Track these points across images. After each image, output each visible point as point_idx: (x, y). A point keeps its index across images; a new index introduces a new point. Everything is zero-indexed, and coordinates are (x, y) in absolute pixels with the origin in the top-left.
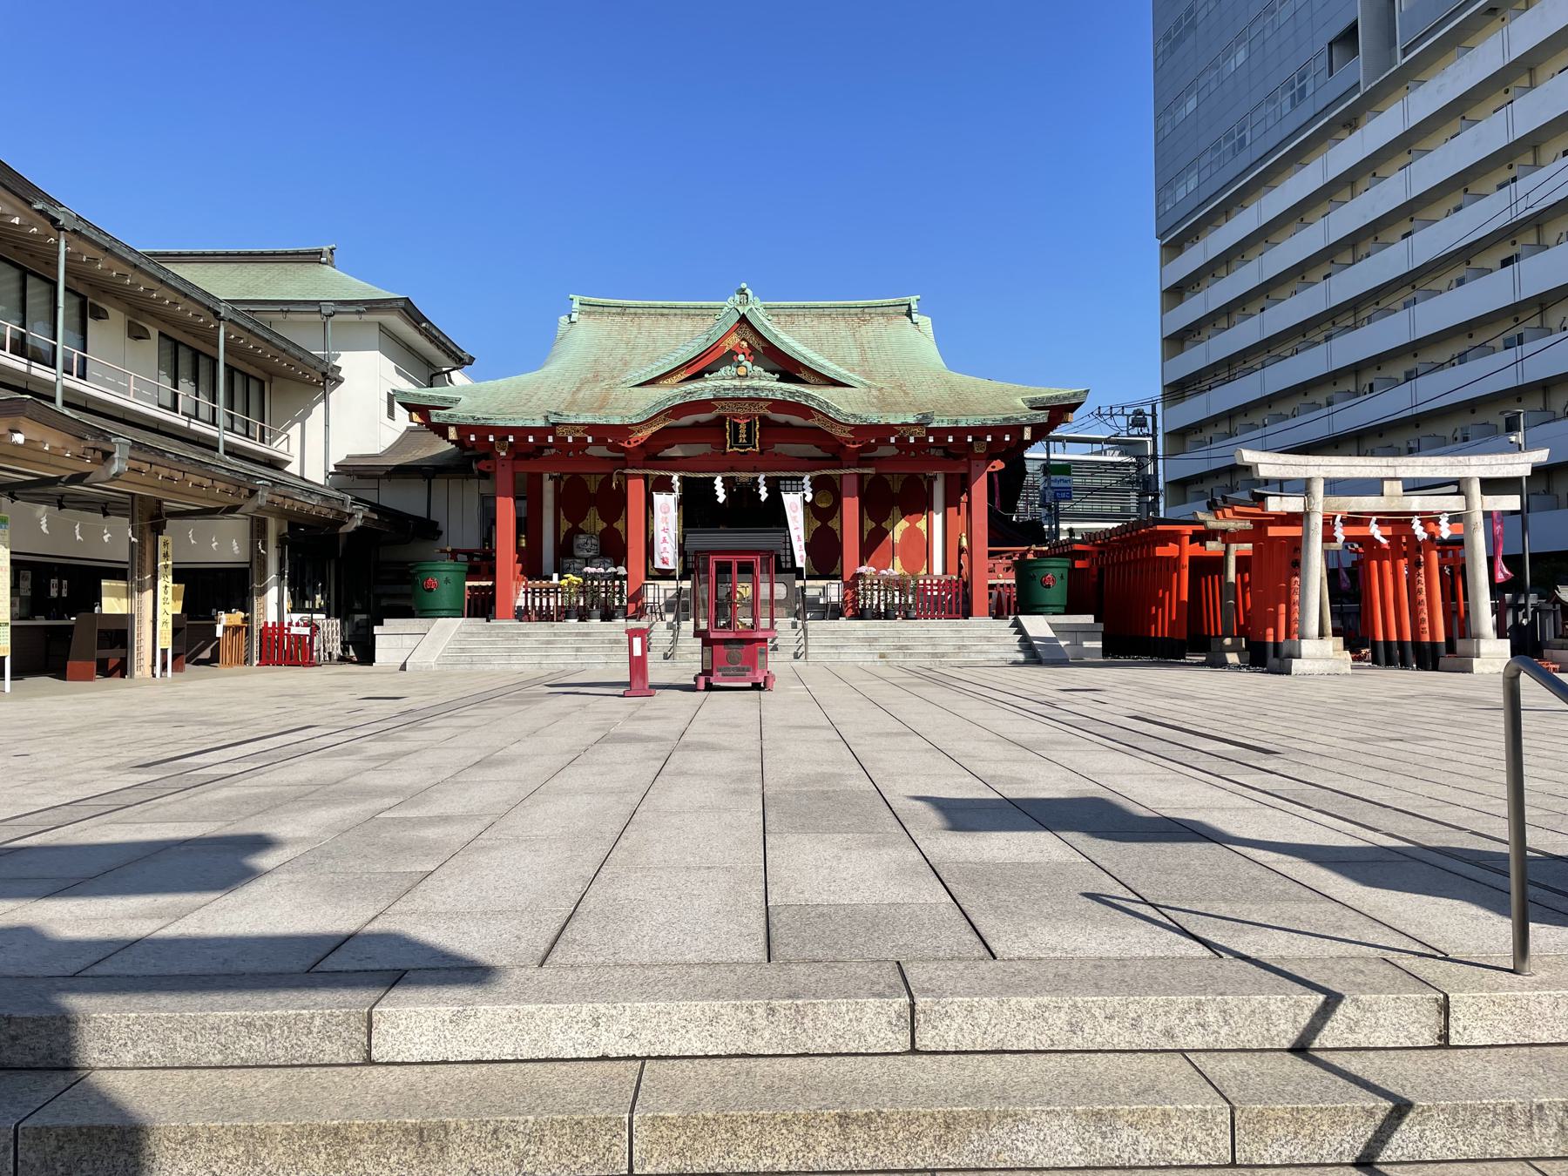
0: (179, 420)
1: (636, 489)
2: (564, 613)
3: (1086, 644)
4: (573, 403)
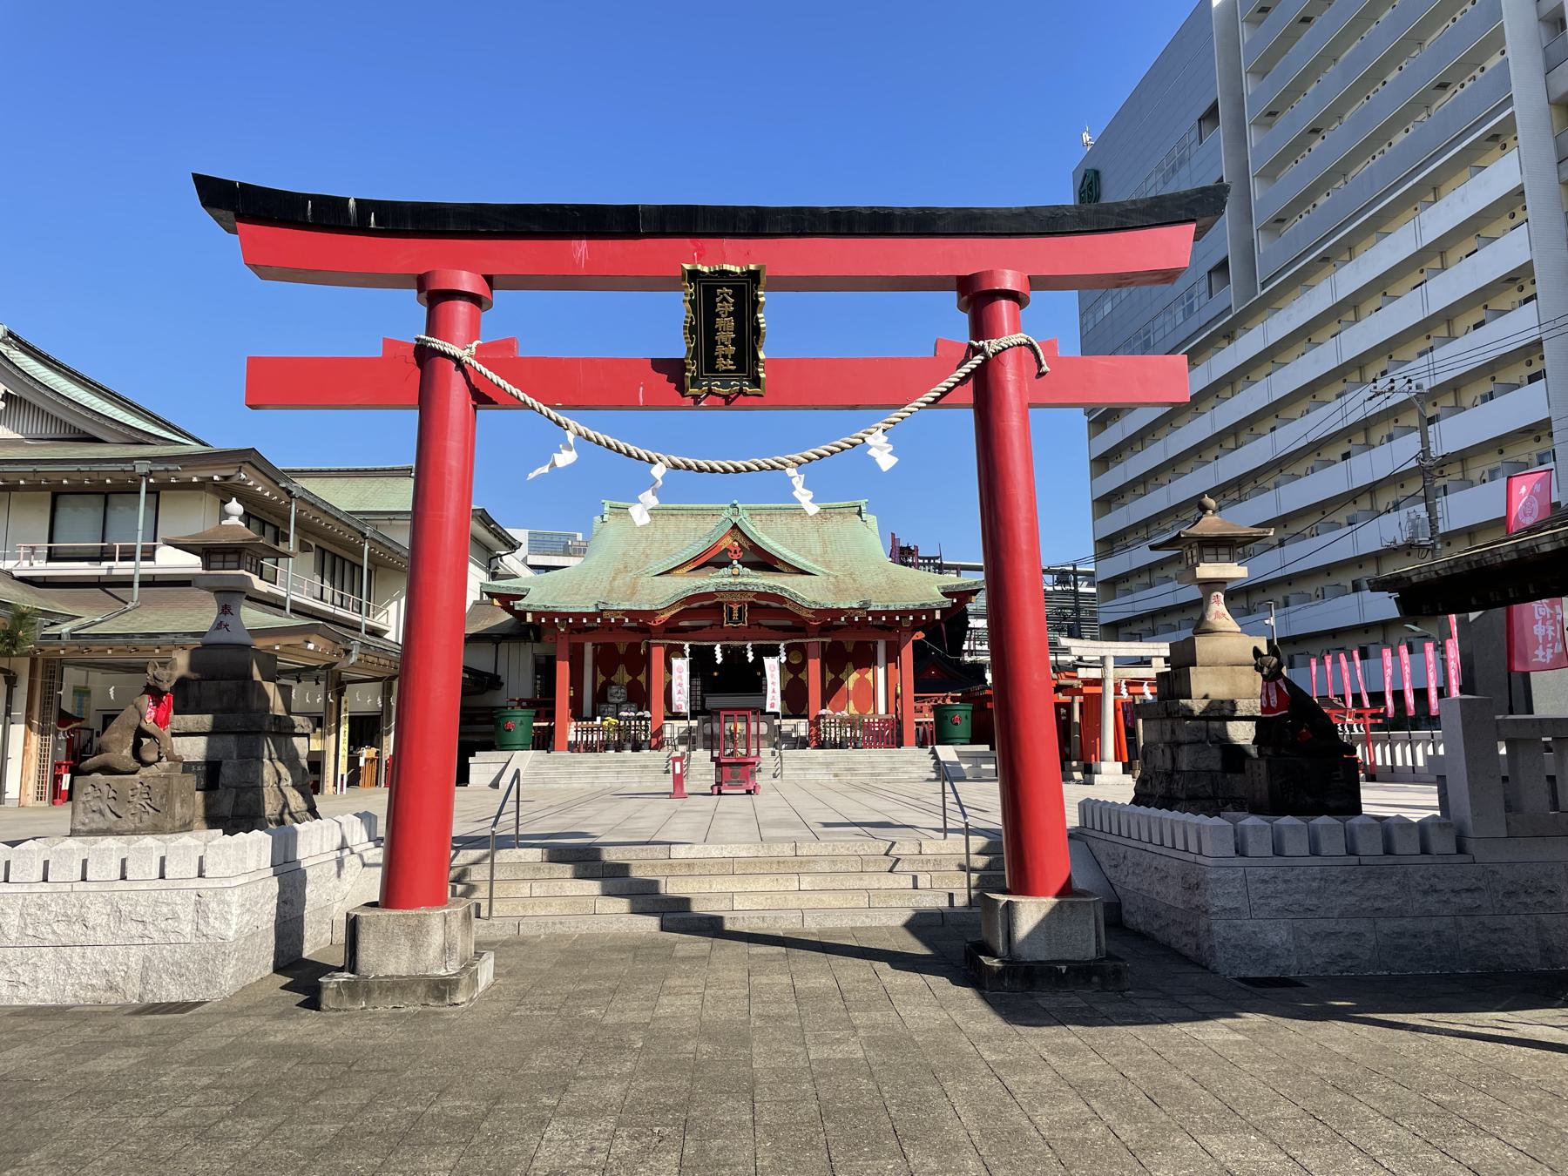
0: (329, 608)
1: (658, 654)
2: (605, 746)
3: (984, 766)
4: (611, 590)
